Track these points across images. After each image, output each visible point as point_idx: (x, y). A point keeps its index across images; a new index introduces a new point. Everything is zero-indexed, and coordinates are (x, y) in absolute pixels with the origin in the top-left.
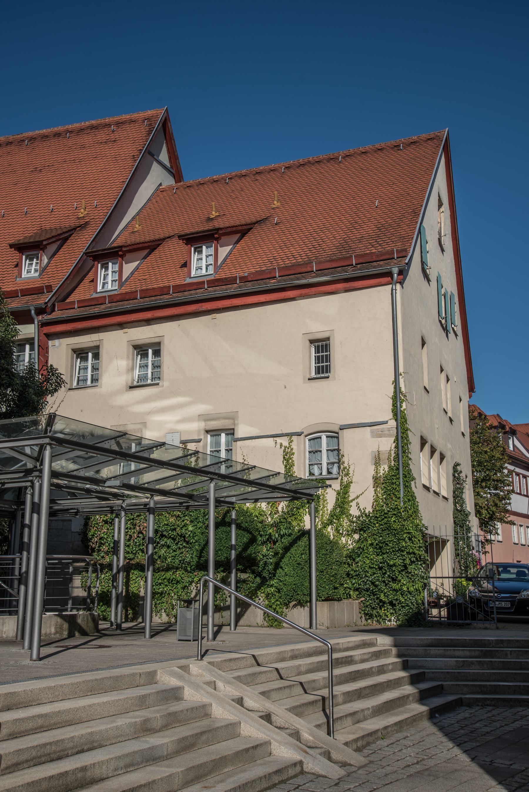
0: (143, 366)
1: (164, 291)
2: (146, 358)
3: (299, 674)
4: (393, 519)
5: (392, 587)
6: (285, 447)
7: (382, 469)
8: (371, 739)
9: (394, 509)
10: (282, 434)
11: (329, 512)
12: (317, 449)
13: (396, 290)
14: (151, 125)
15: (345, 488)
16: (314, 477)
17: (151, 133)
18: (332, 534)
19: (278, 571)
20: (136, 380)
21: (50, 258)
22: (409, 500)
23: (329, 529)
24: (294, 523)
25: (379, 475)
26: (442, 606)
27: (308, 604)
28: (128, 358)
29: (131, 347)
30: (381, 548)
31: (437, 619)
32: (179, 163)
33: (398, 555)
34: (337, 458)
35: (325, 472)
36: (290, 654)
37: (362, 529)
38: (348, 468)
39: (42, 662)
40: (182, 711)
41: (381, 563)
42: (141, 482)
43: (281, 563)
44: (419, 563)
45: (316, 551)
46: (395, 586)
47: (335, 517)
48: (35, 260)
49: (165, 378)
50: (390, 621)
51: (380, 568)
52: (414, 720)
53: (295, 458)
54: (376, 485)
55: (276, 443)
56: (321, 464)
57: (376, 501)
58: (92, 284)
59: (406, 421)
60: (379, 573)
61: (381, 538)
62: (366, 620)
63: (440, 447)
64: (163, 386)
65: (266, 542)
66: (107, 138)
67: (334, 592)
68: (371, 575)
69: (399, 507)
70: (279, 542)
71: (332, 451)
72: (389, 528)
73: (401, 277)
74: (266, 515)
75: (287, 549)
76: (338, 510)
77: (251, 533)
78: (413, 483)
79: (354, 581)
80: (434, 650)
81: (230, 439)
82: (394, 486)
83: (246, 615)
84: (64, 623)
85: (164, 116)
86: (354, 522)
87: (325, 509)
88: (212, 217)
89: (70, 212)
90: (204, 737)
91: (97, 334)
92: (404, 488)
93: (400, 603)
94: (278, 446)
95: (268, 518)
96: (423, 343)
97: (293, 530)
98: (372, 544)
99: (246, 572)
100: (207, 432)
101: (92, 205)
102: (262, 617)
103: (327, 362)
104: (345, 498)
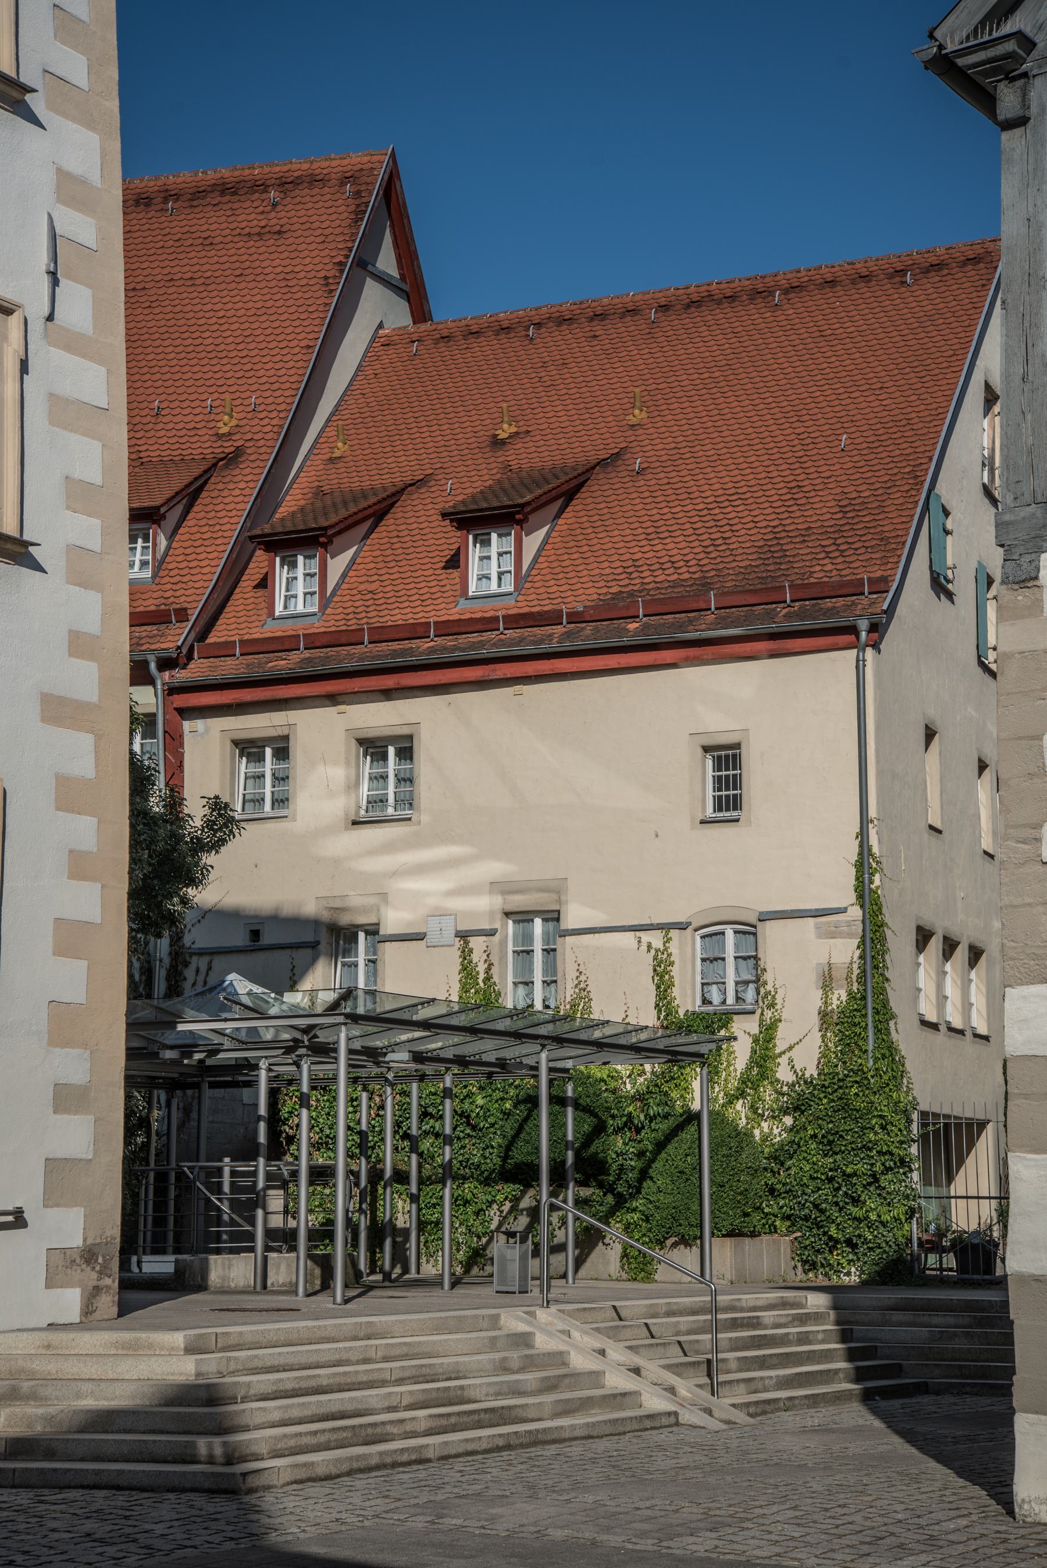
0: (376, 778)
1: (417, 631)
2: (381, 762)
3: (677, 1334)
4: (854, 1090)
5: (850, 1214)
6: (657, 951)
7: (835, 997)
8: (768, 1408)
9: (856, 1073)
10: (652, 925)
11: (738, 1074)
12: (717, 955)
13: (864, 661)
14: (358, 194)
15: (768, 1033)
16: (710, 1009)
17: (362, 219)
18: (743, 1115)
19: (645, 1185)
20: (364, 808)
21: (171, 537)
22: (884, 1056)
23: (739, 1105)
24: (674, 1095)
25: (830, 1008)
26: (945, 1250)
27: (698, 1242)
28: (348, 763)
29: (354, 742)
30: (830, 1143)
31: (934, 1273)
32: (419, 267)
33: (862, 1156)
34: (754, 972)
35: (731, 1000)
36: (664, 1309)
37: (798, 1107)
38: (773, 993)
39: (349, 1306)
40: (538, 1355)
41: (831, 1170)
42: (378, 1010)
43: (651, 1171)
44: (901, 1171)
45: (711, 1151)
46: (855, 1211)
47: (750, 1085)
48: (140, 540)
49: (422, 806)
50: (848, 1274)
51: (831, 1180)
52: (838, 1398)
53: (675, 971)
54: (825, 1026)
55: (639, 942)
56: (724, 983)
57: (824, 1055)
58: (261, 592)
59: (880, 909)
60: (826, 1190)
61: (830, 1126)
62: (806, 1272)
63: (967, 931)
64: (419, 823)
65: (623, 1129)
66: (263, 223)
67: (744, 1222)
68: (813, 1192)
69: (865, 1070)
70: (646, 1130)
71: (745, 958)
72: (845, 1107)
73: (875, 636)
74: (622, 1078)
75: (660, 1146)
76: (756, 1071)
77: (596, 1116)
78: (892, 1023)
79: (782, 1203)
80: (897, 1316)
81: (551, 929)
82: (858, 1030)
83: (589, 1260)
84: (315, 1267)
85: (388, 171)
86: (783, 1095)
87: (732, 1068)
88: (503, 435)
89: (197, 419)
90: (567, 1381)
91: (284, 713)
92: (875, 1034)
93: (866, 1241)
94: (644, 947)
95: (625, 1083)
96: (930, 734)
97: (673, 1107)
98: (814, 1136)
99: (589, 1186)
100: (507, 914)
101: (246, 402)
102: (618, 1264)
103: (735, 789)
104: (767, 1049)
